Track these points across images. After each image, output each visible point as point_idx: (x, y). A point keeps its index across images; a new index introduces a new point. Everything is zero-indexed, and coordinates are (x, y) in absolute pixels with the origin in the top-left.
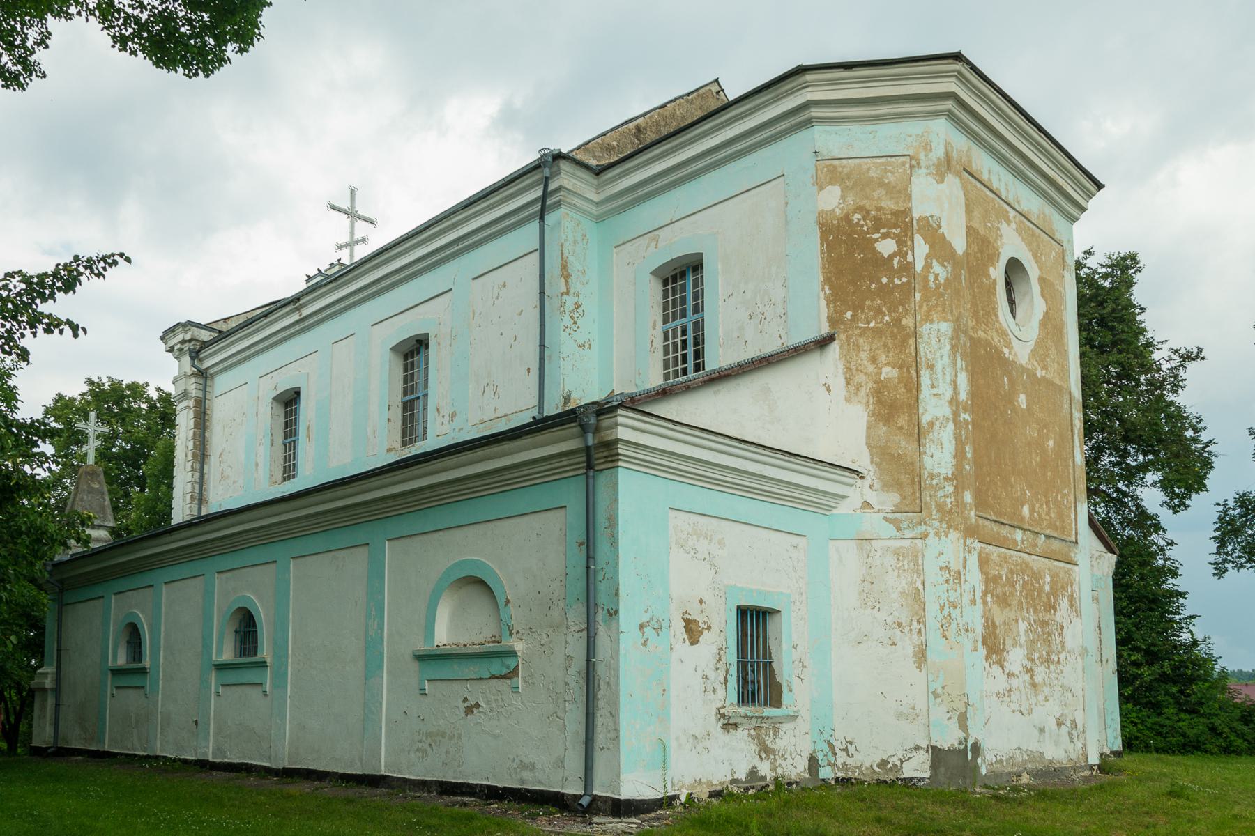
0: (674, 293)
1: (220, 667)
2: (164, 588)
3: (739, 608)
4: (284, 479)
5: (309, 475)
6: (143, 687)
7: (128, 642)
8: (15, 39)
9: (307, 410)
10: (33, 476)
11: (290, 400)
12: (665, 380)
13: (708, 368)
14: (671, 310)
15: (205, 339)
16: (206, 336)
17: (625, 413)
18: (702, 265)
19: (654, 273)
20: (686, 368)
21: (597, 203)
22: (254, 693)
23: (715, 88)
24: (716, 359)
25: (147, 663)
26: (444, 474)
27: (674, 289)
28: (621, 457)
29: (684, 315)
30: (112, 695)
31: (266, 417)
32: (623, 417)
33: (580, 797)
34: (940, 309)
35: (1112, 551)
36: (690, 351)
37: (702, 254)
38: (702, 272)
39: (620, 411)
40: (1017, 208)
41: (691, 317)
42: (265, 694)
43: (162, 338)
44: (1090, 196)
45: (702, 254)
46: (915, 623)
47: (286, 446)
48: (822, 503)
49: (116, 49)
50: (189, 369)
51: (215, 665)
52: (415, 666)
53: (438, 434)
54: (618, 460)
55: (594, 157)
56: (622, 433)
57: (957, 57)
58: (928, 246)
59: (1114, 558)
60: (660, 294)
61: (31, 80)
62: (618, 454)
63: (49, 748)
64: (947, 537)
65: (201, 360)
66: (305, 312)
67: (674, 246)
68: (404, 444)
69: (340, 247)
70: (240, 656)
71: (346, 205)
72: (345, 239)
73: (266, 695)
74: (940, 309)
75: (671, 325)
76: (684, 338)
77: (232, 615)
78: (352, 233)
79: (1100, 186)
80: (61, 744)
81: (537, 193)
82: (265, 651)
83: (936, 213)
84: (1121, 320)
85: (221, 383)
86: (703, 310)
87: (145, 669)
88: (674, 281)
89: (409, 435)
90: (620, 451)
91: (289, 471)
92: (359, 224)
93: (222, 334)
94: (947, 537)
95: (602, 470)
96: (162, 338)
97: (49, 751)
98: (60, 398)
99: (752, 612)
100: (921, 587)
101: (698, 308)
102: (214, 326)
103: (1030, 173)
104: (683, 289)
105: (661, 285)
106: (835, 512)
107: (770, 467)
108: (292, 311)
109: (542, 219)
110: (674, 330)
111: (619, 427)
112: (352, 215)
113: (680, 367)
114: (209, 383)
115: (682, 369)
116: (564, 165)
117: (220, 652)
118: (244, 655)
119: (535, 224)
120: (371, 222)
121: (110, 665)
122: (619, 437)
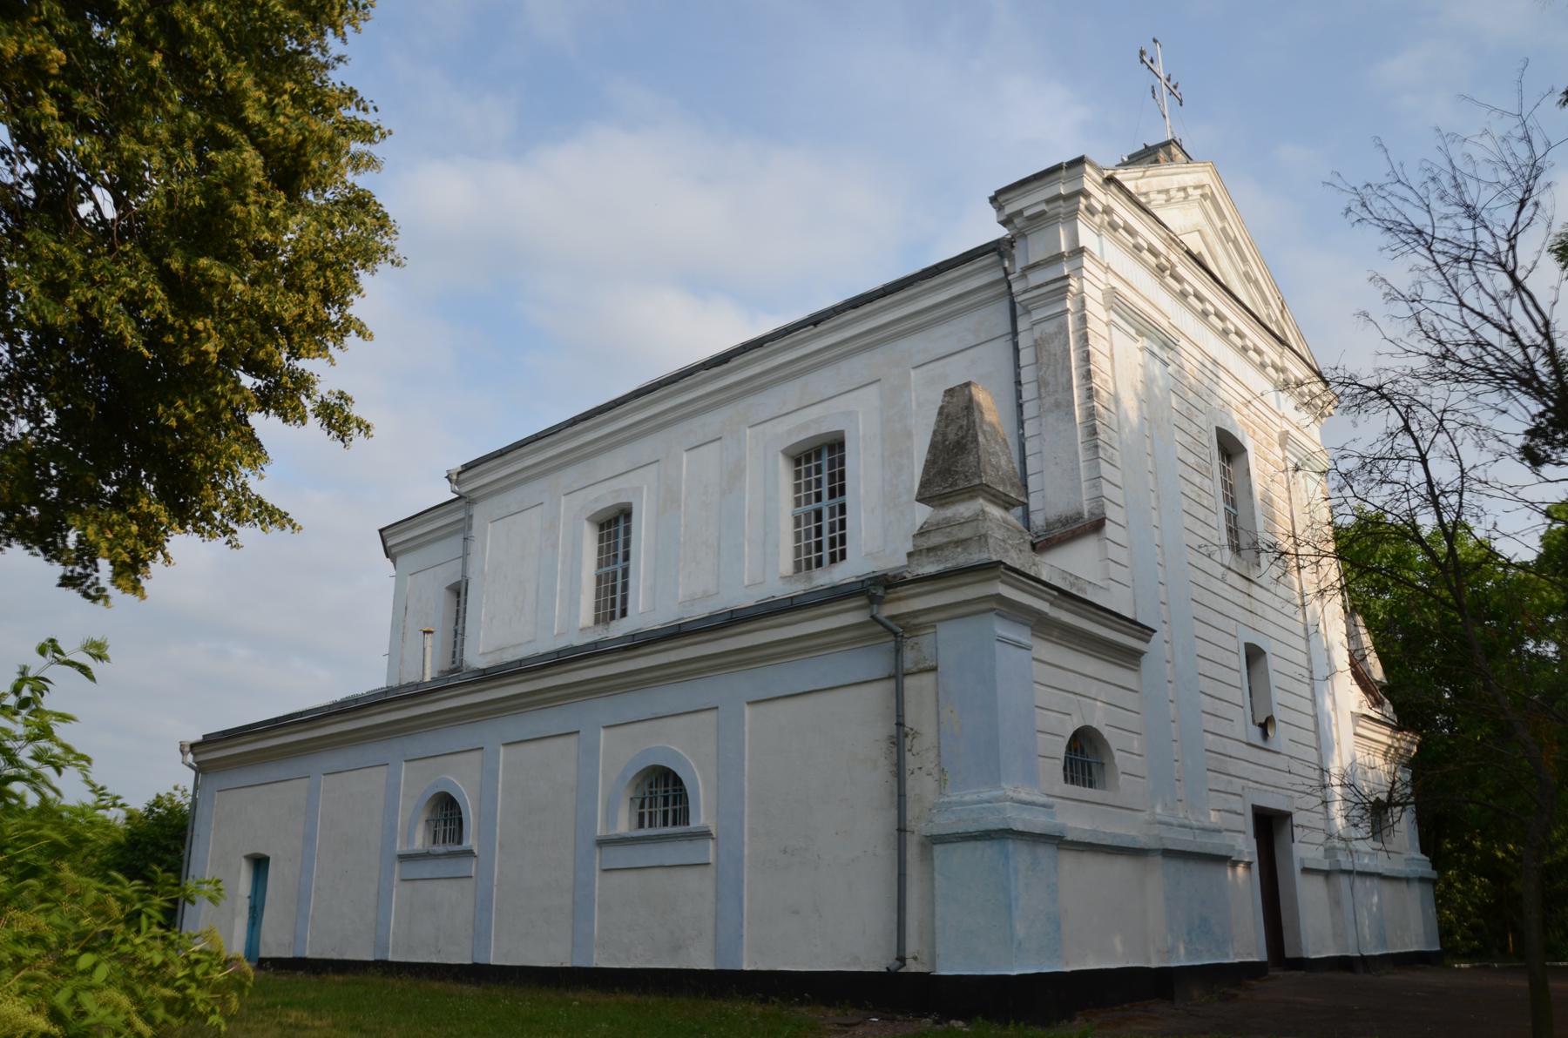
0: (808, 474)
8: (278, 135)
14: (806, 490)
19: (785, 452)
25: (470, 841)
29: (615, 563)
43: (993, 200)
53: (478, 655)
67: (605, 498)
88: (808, 460)
89: (808, 560)
96: (993, 200)
101: (627, 557)
104: (819, 470)
110: (807, 515)
117: (409, 838)
121: (398, 849)
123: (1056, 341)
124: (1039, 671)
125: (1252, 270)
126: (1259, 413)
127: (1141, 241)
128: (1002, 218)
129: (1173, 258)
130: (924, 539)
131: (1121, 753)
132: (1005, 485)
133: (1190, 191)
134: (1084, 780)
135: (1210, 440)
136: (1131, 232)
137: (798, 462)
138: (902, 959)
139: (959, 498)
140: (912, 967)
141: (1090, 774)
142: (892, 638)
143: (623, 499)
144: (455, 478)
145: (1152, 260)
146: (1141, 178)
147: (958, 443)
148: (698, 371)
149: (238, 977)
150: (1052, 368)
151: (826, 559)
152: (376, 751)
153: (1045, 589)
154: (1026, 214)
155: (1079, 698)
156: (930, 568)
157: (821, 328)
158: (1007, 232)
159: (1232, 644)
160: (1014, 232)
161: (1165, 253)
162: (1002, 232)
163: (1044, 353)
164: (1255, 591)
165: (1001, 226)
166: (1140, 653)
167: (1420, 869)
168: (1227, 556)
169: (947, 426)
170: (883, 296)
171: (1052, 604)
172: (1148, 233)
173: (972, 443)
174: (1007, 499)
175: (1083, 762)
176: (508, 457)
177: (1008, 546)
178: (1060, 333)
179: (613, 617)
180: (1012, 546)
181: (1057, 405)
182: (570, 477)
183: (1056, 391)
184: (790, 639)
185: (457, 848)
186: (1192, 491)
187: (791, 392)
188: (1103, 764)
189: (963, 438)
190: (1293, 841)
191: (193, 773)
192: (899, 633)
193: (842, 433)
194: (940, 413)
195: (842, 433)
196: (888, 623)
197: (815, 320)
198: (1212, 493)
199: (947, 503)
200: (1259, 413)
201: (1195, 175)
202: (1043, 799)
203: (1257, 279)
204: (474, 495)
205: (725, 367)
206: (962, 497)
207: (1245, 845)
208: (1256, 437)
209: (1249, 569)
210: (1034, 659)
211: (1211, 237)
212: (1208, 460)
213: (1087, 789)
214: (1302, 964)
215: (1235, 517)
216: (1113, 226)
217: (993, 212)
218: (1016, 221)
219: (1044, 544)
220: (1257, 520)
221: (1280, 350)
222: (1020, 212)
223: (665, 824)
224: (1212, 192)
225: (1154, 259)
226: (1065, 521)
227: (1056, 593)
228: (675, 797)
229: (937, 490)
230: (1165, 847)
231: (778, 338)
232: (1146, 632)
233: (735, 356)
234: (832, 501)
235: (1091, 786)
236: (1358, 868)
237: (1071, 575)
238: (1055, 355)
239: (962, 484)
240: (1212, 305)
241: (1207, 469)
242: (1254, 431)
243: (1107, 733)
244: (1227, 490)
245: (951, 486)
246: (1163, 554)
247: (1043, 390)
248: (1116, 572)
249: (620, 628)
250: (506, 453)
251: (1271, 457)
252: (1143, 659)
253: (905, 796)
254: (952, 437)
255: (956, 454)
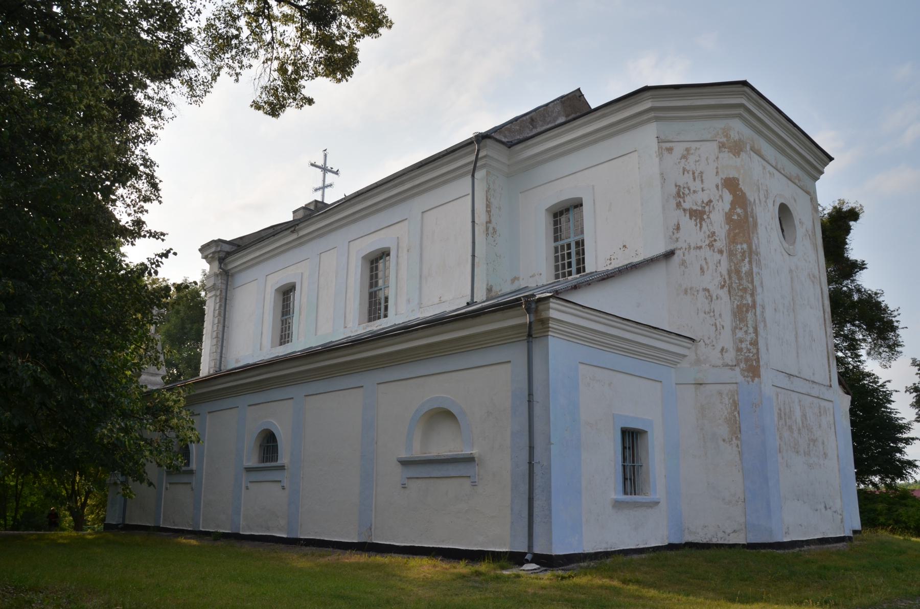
1: (249, 470)
2: (208, 416)
3: (622, 428)
4: (281, 344)
5: (300, 343)
6: (190, 483)
7: (260, 446)
9: (299, 299)
11: (287, 293)
12: (556, 278)
13: (587, 271)
15: (229, 250)
16: (227, 248)
17: (554, 301)
20: (571, 271)
21: (509, 165)
22: (276, 487)
23: (578, 94)
24: (594, 263)
28: (550, 329)
30: (167, 489)
32: (553, 304)
33: (525, 554)
34: (741, 235)
35: (848, 393)
36: (574, 260)
39: (551, 300)
40: (783, 172)
42: (283, 488)
44: (826, 164)
46: (734, 439)
47: (282, 321)
48: (672, 360)
49: (349, 78)
50: (216, 270)
51: (246, 468)
52: (399, 468)
54: (548, 331)
55: (505, 137)
56: (553, 314)
58: (731, 196)
59: (849, 397)
60: (552, 223)
62: (549, 327)
63: (120, 524)
64: (753, 382)
65: (226, 265)
66: (301, 233)
68: (370, 320)
69: (316, 190)
70: (263, 462)
71: (320, 163)
72: (321, 185)
73: (284, 489)
74: (741, 235)
76: (569, 251)
77: (261, 432)
78: (324, 181)
79: (831, 159)
80: (127, 522)
81: (472, 158)
82: (284, 457)
83: (736, 176)
85: (241, 279)
87: (192, 471)
90: (550, 325)
91: (284, 337)
92: (329, 175)
93: (241, 245)
94: (753, 382)
95: (536, 338)
97: (120, 526)
99: (629, 432)
100: (737, 415)
102: (235, 242)
103: (788, 151)
105: (552, 216)
106: (679, 365)
107: (640, 336)
108: (292, 232)
109: (473, 176)
110: (562, 247)
111: (550, 310)
112: (325, 169)
113: (567, 270)
114: (230, 279)
115: (568, 271)
116: (489, 142)
118: (267, 462)
119: (469, 178)
120: (337, 173)
122: (551, 315)
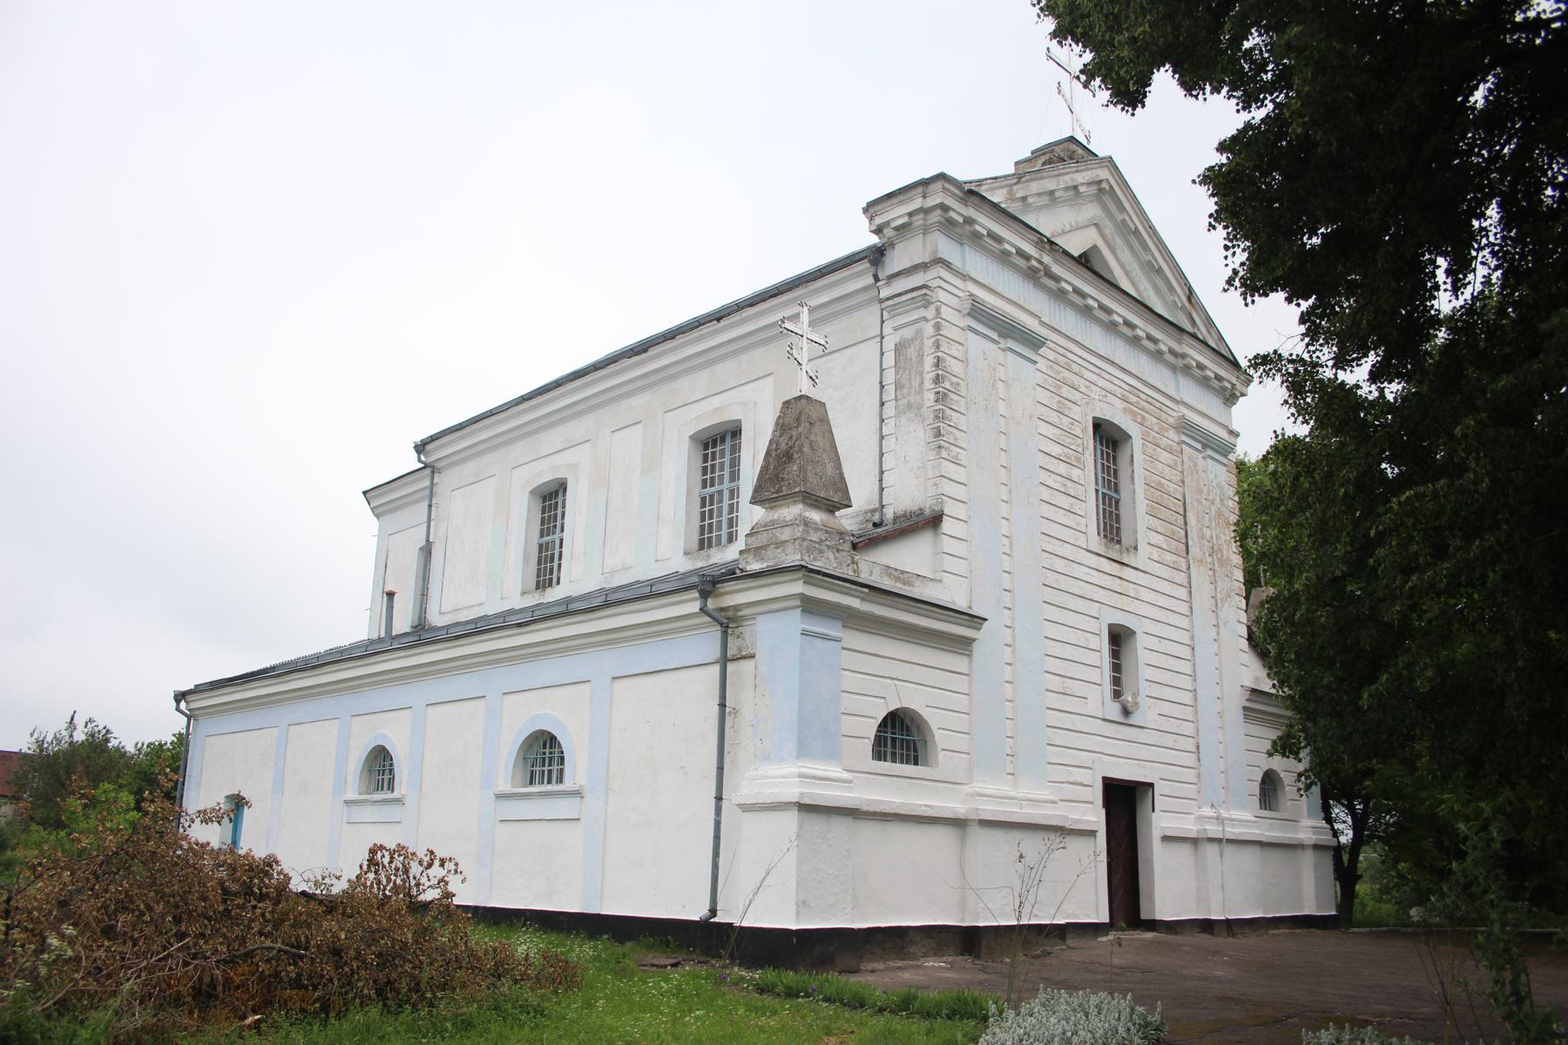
0: (714, 459)
10: (1404, 493)
11: (551, 498)
18: (740, 430)
26: (915, 616)
27: (714, 454)
29: (721, 482)
31: (521, 516)
37: (740, 420)
38: (740, 438)
41: (726, 485)
43: (865, 210)
45: (740, 420)
57: (942, 177)
61: (143, 744)
67: (544, 473)
75: (709, 490)
84: (1229, 561)
86: (739, 479)
88: (714, 446)
98: (1211, 178)
123: (912, 347)
124: (848, 659)
125: (1155, 259)
126: (1150, 400)
127: (1007, 247)
128: (874, 228)
129: (1046, 259)
130: (754, 539)
131: (941, 731)
132: (827, 490)
133: (1082, 189)
134: (894, 754)
135: (1084, 430)
136: (998, 239)
137: (706, 447)
138: (713, 912)
139: (783, 502)
140: (720, 918)
141: (915, 750)
142: (719, 628)
143: (560, 475)
144: (421, 448)
145: (1021, 262)
146: (1016, 184)
147: (787, 452)
148: (622, 359)
149: (413, 883)
150: (907, 372)
151: (95, 724)
152: (328, 705)
153: (854, 587)
154: (893, 225)
155: (896, 682)
156: (755, 566)
157: (723, 323)
158: (879, 240)
159: (1092, 625)
160: (884, 240)
161: (1036, 256)
162: (874, 240)
163: (901, 358)
164: (1128, 573)
165: (873, 235)
166: (968, 642)
167: (1314, 837)
168: (1096, 543)
169: (780, 436)
170: (774, 296)
171: (863, 599)
172: (1014, 240)
173: (797, 453)
174: (830, 503)
175: (908, 741)
176: (467, 430)
177: (824, 547)
178: (916, 339)
179: (550, 585)
180: (828, 547)
181: (909, 406)
182: (518, 451)
183: (909, 394)
184: (635, 625)
185: (389, 796)
186: (1055, 481)
187: (700, 382)
188: (926, 741)
189: (791, 448)
190: (1153, 811)
191: (186, 719)
192: (728, 622)
193: (566, 479)
194: (777, 424)
195: (566, 479)
196: (716, 614)
197: (718, 316)
198: (1082, 482)
199: (775, 506)
200: (1150, 400)
201: (1089, 173)
202: (846, 775)
203: (1160, 268)
204: (439, 465)
205: (644, 356)
206: (787, 501)
207: (1094, 816)
208: (1146, 423)
209: (1121, 553)
210: (844, 648)
211: (1109, 228)
212: (1080, 450)
213: (882, 762)
214: (1153, 925)
215: (1117, 502)
216: (976, 236)
217: (866, 221)
218: (885, 231)
219: (863, 543)
220: (1137, 505)
221: (1179, 337)
222: (888, 223)
223: (549, 782)
224: (1111, 187)
225: (1025, 262)
226: (907, 516)
227: (867, 590)
228: (550, 759)
229: (767, 495)
230: (981, 818)
231: (687, 331)
232: (976, 620)
233: (652, 346)
234: (732, 485)
235: (916, 763)
236: (1228, 836)
237: (896, 570)
238: (911, 359)
239: (785, 491)
240: (1096, 300)
241: (1078, 460)
242: (1143, 418)
243: (926, 714)
244: (1109, 475)
245: (776, 492)
246: (1011, 544)
247: (899, 393)
248: (949, 563)
249: (554, 594)
250: (464, 427)
251: (1164, 442)
252: (974, 644)
253: (718, 768)
254: (783, 446)
255: (785, 463)
